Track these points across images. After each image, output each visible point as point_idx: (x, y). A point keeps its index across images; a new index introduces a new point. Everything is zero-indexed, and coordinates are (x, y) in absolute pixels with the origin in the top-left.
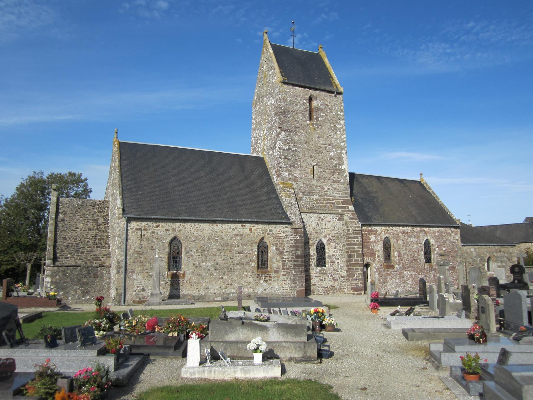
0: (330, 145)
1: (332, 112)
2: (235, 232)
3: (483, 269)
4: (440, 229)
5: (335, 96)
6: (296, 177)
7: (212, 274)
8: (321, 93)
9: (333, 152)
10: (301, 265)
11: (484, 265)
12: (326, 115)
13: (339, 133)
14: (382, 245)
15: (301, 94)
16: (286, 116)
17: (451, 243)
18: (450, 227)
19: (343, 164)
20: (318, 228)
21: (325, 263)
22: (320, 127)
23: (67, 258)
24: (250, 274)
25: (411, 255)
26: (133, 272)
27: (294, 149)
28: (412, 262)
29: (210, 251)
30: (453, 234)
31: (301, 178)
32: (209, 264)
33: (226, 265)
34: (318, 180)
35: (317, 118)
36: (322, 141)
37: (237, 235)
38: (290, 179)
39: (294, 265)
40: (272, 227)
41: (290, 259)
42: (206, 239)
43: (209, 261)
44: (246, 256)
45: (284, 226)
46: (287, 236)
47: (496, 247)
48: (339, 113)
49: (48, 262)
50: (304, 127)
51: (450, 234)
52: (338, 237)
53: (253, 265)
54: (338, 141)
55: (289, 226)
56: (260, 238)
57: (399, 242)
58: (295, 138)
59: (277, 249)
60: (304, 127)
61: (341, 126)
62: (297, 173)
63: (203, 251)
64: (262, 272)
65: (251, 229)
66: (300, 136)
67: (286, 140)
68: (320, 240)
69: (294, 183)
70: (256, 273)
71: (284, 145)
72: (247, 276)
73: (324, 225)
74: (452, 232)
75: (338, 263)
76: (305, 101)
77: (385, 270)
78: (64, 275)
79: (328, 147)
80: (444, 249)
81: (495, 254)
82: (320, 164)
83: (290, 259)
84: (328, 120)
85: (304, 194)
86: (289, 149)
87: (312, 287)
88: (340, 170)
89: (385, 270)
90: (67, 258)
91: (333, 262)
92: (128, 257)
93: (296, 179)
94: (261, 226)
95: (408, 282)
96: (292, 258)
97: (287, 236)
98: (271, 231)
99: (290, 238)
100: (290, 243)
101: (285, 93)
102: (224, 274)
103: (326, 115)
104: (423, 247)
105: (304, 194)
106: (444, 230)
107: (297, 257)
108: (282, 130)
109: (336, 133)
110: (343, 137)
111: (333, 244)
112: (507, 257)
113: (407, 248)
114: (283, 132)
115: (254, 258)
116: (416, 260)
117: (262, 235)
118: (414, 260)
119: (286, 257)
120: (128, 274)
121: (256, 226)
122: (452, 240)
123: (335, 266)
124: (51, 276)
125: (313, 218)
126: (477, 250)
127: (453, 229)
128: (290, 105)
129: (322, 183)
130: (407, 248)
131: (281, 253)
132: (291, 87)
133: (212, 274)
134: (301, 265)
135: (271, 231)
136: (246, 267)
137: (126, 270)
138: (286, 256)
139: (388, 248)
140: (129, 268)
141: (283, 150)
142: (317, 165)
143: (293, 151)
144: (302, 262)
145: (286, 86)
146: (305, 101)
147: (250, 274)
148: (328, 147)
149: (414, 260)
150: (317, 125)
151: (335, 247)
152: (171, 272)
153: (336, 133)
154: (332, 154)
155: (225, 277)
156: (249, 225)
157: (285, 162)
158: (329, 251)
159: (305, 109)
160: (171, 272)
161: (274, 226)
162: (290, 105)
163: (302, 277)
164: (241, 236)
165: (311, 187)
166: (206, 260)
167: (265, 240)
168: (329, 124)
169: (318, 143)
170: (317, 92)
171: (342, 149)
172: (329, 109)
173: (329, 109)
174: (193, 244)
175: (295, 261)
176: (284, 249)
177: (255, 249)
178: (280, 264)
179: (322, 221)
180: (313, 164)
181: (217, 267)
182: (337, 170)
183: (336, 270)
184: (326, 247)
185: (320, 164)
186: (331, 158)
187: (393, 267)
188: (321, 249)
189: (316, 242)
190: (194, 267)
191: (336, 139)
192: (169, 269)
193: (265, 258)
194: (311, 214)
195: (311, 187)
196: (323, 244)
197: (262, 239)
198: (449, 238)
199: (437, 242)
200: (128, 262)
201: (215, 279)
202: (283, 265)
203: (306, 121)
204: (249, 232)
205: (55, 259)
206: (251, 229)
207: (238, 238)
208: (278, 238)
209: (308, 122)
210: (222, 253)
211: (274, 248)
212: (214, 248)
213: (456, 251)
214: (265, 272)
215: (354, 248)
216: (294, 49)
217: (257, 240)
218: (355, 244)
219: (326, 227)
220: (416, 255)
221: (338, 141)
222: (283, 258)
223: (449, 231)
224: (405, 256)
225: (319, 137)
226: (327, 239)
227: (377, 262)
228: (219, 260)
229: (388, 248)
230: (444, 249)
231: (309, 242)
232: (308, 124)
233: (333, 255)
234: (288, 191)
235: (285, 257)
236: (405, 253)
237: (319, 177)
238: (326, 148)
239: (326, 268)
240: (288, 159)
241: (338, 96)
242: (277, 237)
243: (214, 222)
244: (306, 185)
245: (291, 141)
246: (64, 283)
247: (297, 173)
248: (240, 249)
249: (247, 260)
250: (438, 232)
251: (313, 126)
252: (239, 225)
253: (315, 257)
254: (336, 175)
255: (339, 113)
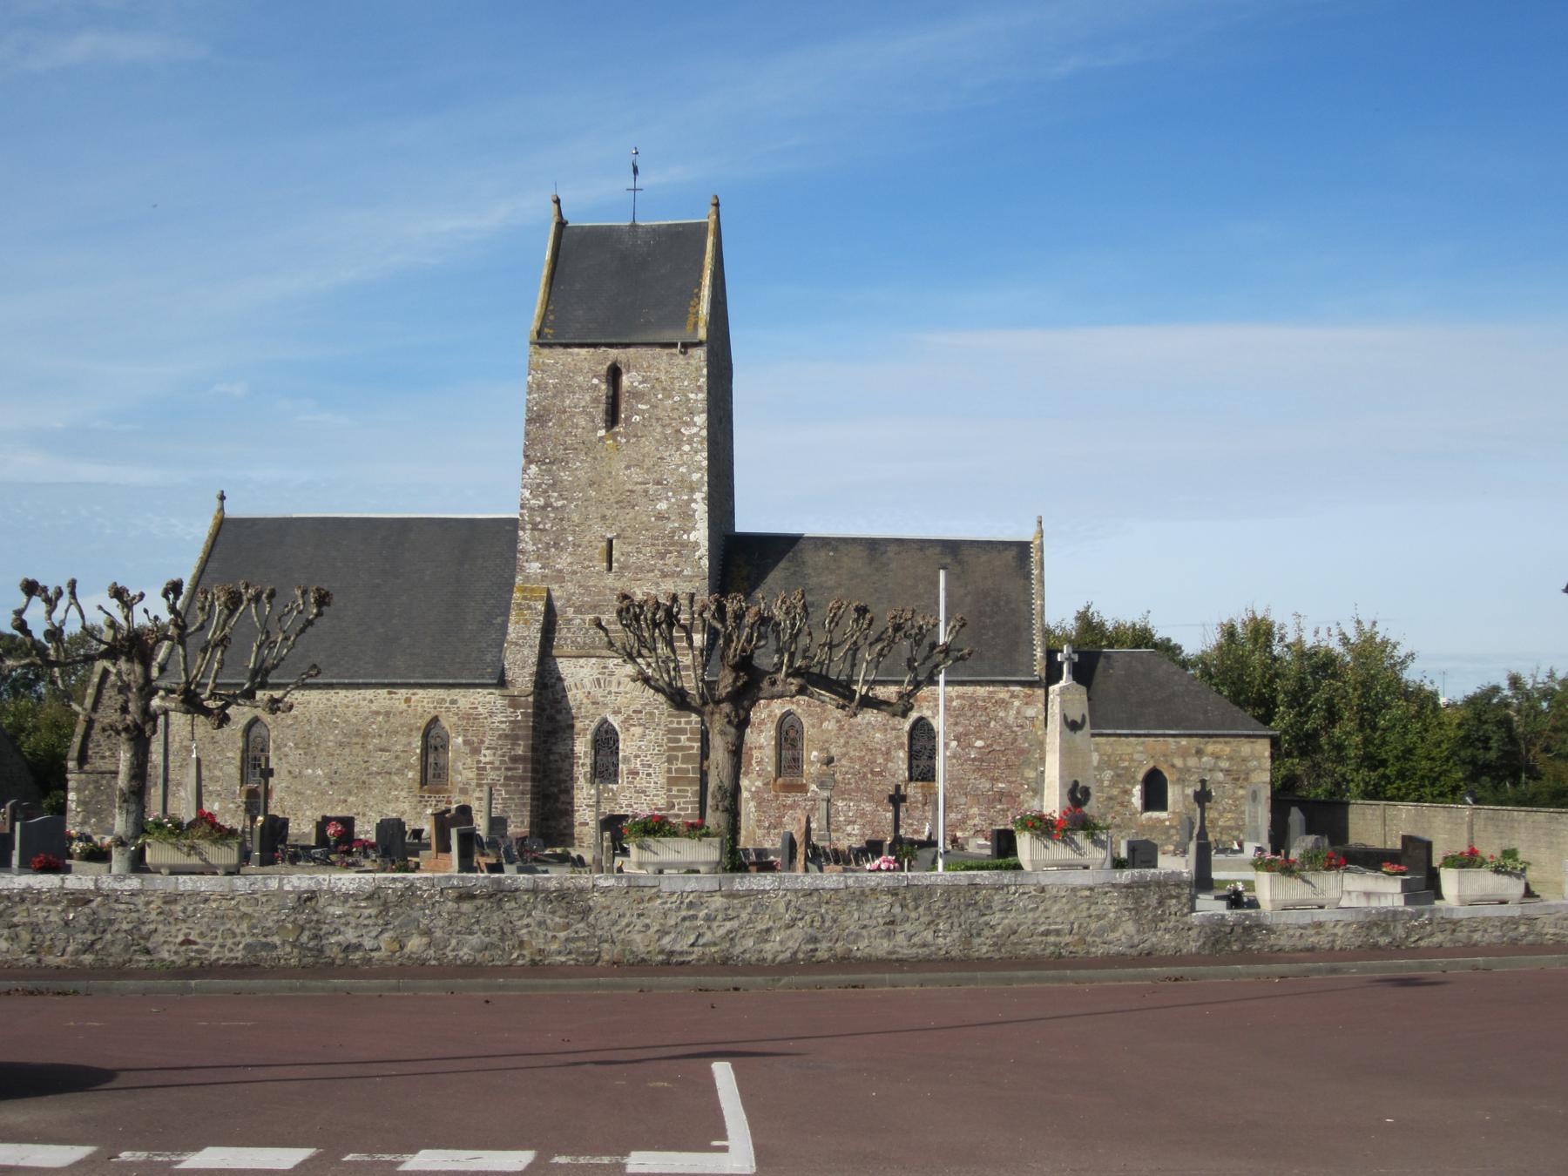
0: (659, 483)
1: (670, 397)
2: (374, 708)
3: (1125, 805)
4: (969, 689)
5: (685, 353)
6: (560, 571)
7: (324, 793)
8: (642, 351)
9: (667, 499)
10: (523, 779)
11: (1127, 792)
12: (654, 407)
13: (686, 448)
14: (773, 733)
15: (586, 365)
16: (543, 424)
17: (1007, 727)
18: (1006, 683)
19: (694, 528)
20: (598, 693)
21: (616, 775)
22: (633, 440)
23: (103, 758)
24: (404, 794)
25: (861, 758)
26: (179, 784)
27: (560, 503)
28: (864, 777)
29: (323, 746)
30: (1017, 703)
31: (575, 573)
32: (320, 772)
33: (353, 775)
34: (620, 576)
35: (628, 418)
36: (636, 474)
37: (377, 713)
38: (544, 577)
39: (506, 778)
40: (456, 694)
41: (497, 764)
42: (315, 721)
43: (320, 766)
44: (397, 757)
45: (486, 691)
46: (491, 714)
47: (1184, 742)
48: (692, 396)
49: (71, 765)
50: (588, 447)
51: (1003, 704)
52: (651, 714)
53: (410, 775)
54: (683, 469)
55: (497, 692)
56: (428, 718)
57: (825, 724)
58: (565, 476)
59: (466, 742)
60: (588, 447)
61: (695, 430)
62: (563, 562)
63: (307, 745)
64: (430, 791)
65: (408, 700)
66: (581, 467)
67: (539, 485)
68: (605, 721)
69: (556, 587)
70: (417, 792)
71: (535, 497)
72: (397, 799)
73: (614, 683)
74: (1013, 696)
75: (649, 775)
76: (595, 381)
77: (777, 797)
78: (97, 788)
79: (652, 488)
80: (979, 743)
81: (1178, 762)
82: (629, 532)
83: (497, 764)
84: (658, 420)
85: (578, 610)
86: (547, 505)
87: (577, 830)
88: (684, 545)
89: (777, 797)
90: (103, 758)
91: (635, 773)
92: (171, 758)
93: (559, 577)
94: (432, 692)
95: (849, 828)
96: (502, 762)
97: (491, 714)
98: (454, 702)
99: (500, 717)
100: (498, 729)
101: (544, 368)
102: (350, 793)
103: (654, 407)
104: (905, 740)
105: (578, 610)
106: (982, 691)
107: (515, 759)
108: (531, 462)
109: (678, 449)
110: (698, 458)
111: (637, 730)
112: (1227, 772)
113: (852, 741)
114: (533, 467)
115: (414, 760)
116: (880, 773)
117: (434, 713)
118: (872, 772)
119: (487, 759)
120: (172, 788)
121: (421, 692)
122: (1011, 720)
123: (641, 782)
124: (78, 790)
125: (585, 670)
126: (1109, 749)
127: (1017, 689)
128: (555, 396)
129: (630, 580)
130: (852, 741)
131: (476, 751)
132: (560, 350)
133: (324, 793)
134: (523, 779)
135: (454, 702)
136: (396, 778)
137: (166, 780)
138: (486, 756)
139: (794, 739)
140: (172, 776)
141: (532, 509)
142: (618, 537)
143: (555, 509)
144: (525, 770)
145: (546, 351)
146: (595, 381)
147: (404, 794)
148: (652, 488)
149: (872, 772)
150: (626, 436)
151: (644, 736)
152: (245, 787)
153: (678, 449)
154: (662, 506)
155: (351, 799)
156: (404, 691)
157: (533, 539)
158: (626, 747)
159: (596, 400)
160: (245, 787)
161: (462, 691)
162: (555, 396)
163: (524, 805)
164: (387, 714)
165: (599, 594)
166: (313, 765)
167: (444, 722)
168: (659, 429)
169: (624, 483)
170: (631, 350)
171: (692, 490)
172: (664, 389)
173: (664, 389)
174: (290, 732)
175: (508, 769)
176: (482, 742)
177: (417, 742)
178: (472, 774)
179: (612, 674)
180: (609, 536)
181: (336, 778)
182: (672, 544)
183: (644, 792)
184: (621, 737)
185: (629, 532)
186: (660, 517)
187: (803, 789)
188: (606, 741)
189: (593, 726)
190: (289, 778)
191: (679, 466)
192: (243, 781)
193: (441, 762)
194: (582, 661)
195: (599, 594)
196: (614, 729)
197: (435, 720)
198: (1002, 714)
199: (956, 724)
200: (171, 765)
201: (331, 802)
202: (480, 776)
203: (595, 430)
204: (403, 706)
205: (83, 759)
206: (408, 700)
207: (380, 718)
208: (470, 717)
209: (602, 433)
210: (347, 750)
211: (460, 740)
212: (331, 739)
213: (1022, 752)
214: (438, 792)
215: (679, 741)
216: (634, 226)
217: (422, 723)
218: (682, 731)
219: (621, 689)
220: (880, 761)
221: (683, 469)
222: (479, 762)
223: (1002, 693)
224: (844, 762)
225: (628, 467)
226: (621, 718)
227: (754, 775)
228: (339, 764)
229: (794, 739)
230: (979, 743)
231: (572, 726)
232: (601, 438)
233: (637, 756)
234: (530, 608)
235: (483, 759)
236: (844, 755)
237: (623, 568)
238: (646, 492)
239: (615, 787)
240: (544, 530)
241: (691, 351)
242: (467, 717)
243: (330, 686)
244: (587, 588)
245: (554, 485)
246: (98, 802)
247: (563, 562)
248: (384, 742)
249: (398, 764)
250: (958, 697)
251: (615, 440)
252: (383, 692)
253: (588, 761)
254: (671, 559)
255: (692, 396)
